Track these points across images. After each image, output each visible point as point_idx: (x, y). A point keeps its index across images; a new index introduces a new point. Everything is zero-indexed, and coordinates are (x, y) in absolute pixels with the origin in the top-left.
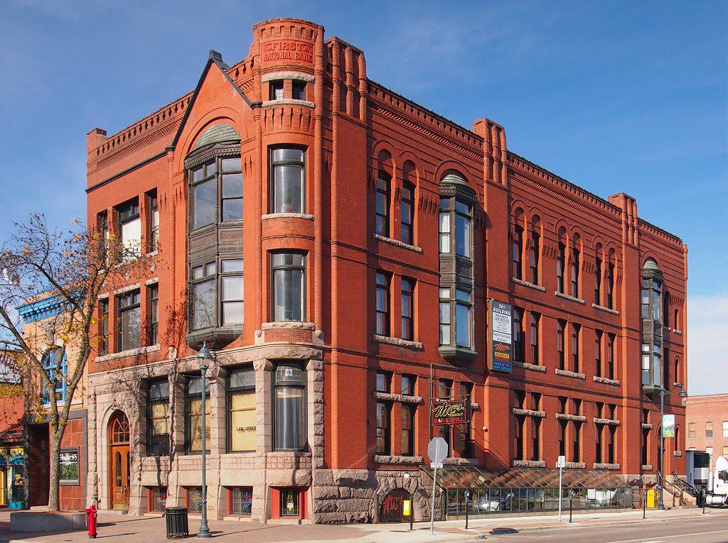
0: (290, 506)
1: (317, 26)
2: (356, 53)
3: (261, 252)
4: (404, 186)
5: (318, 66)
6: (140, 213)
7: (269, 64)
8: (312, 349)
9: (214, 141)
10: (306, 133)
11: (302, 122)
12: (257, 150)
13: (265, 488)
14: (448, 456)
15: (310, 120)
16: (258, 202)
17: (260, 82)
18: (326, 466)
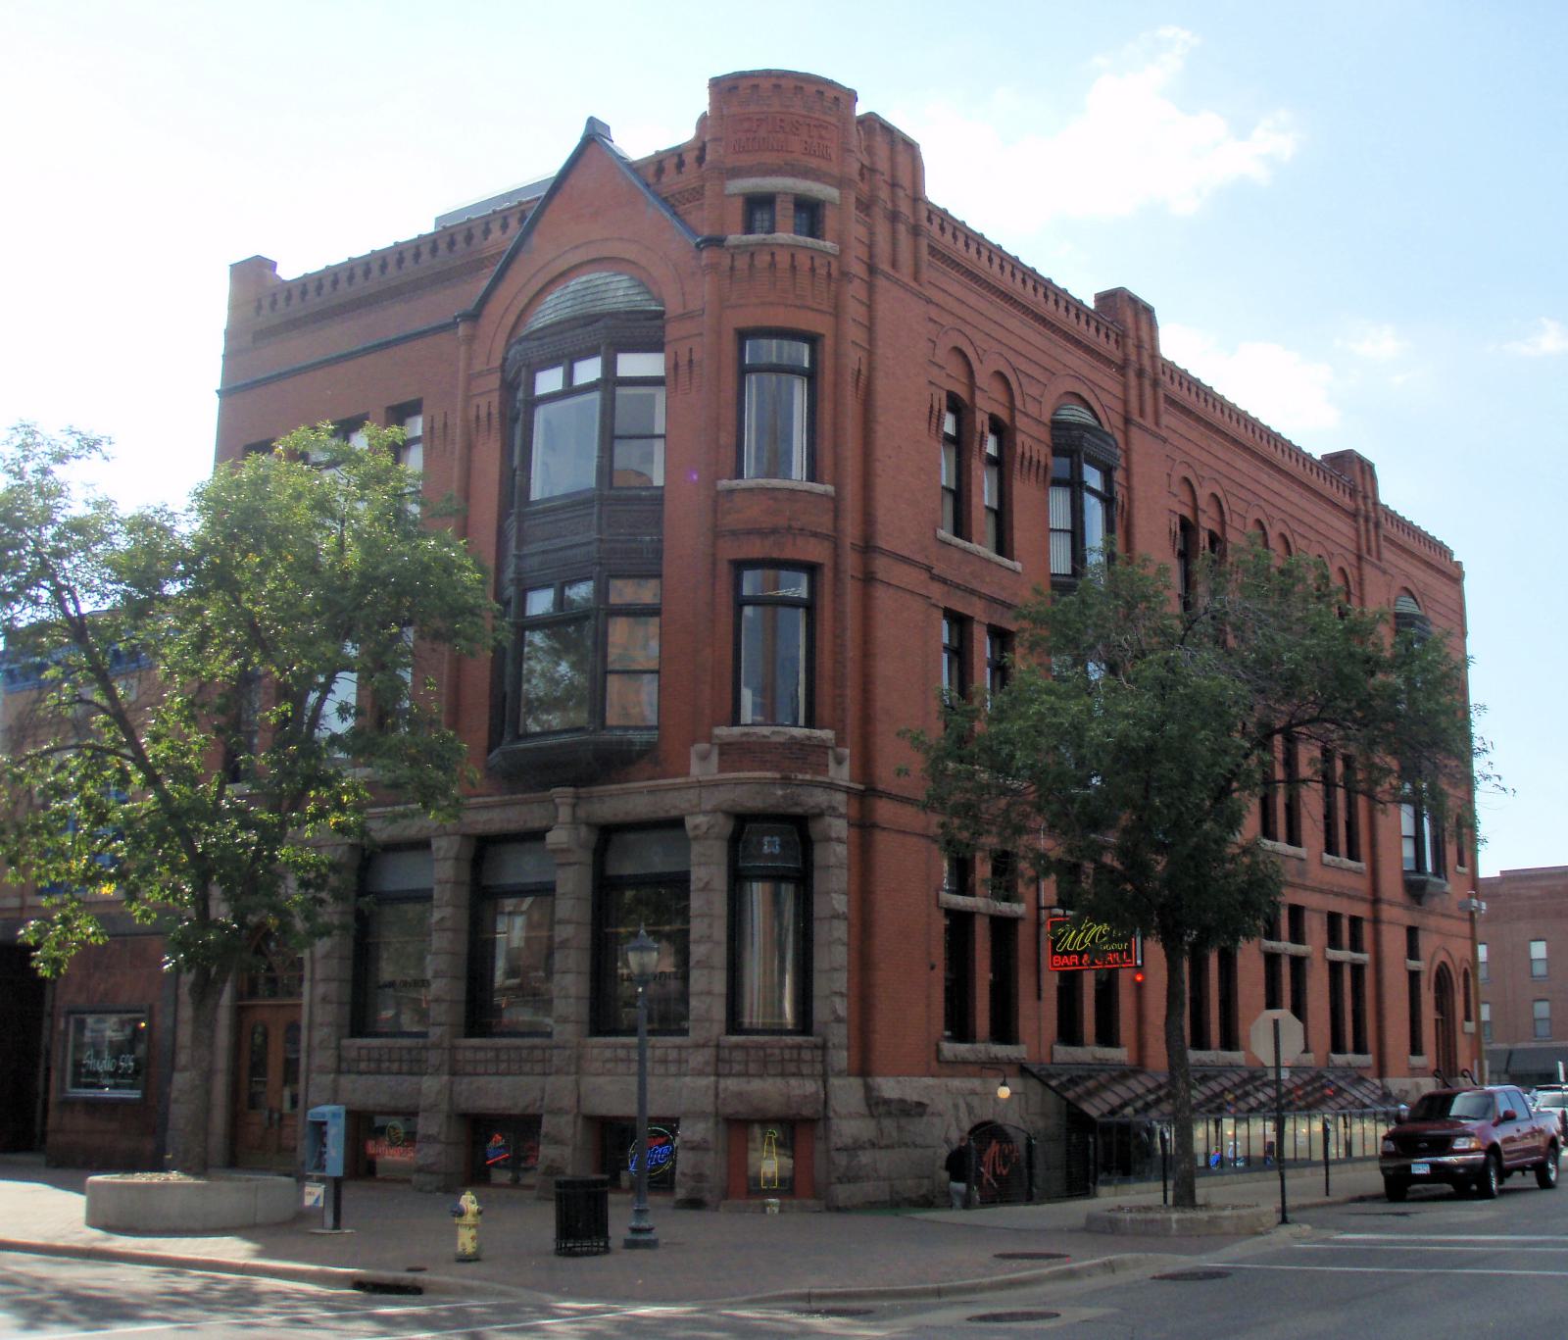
7: (746, 160)
14: (1306, 1050)
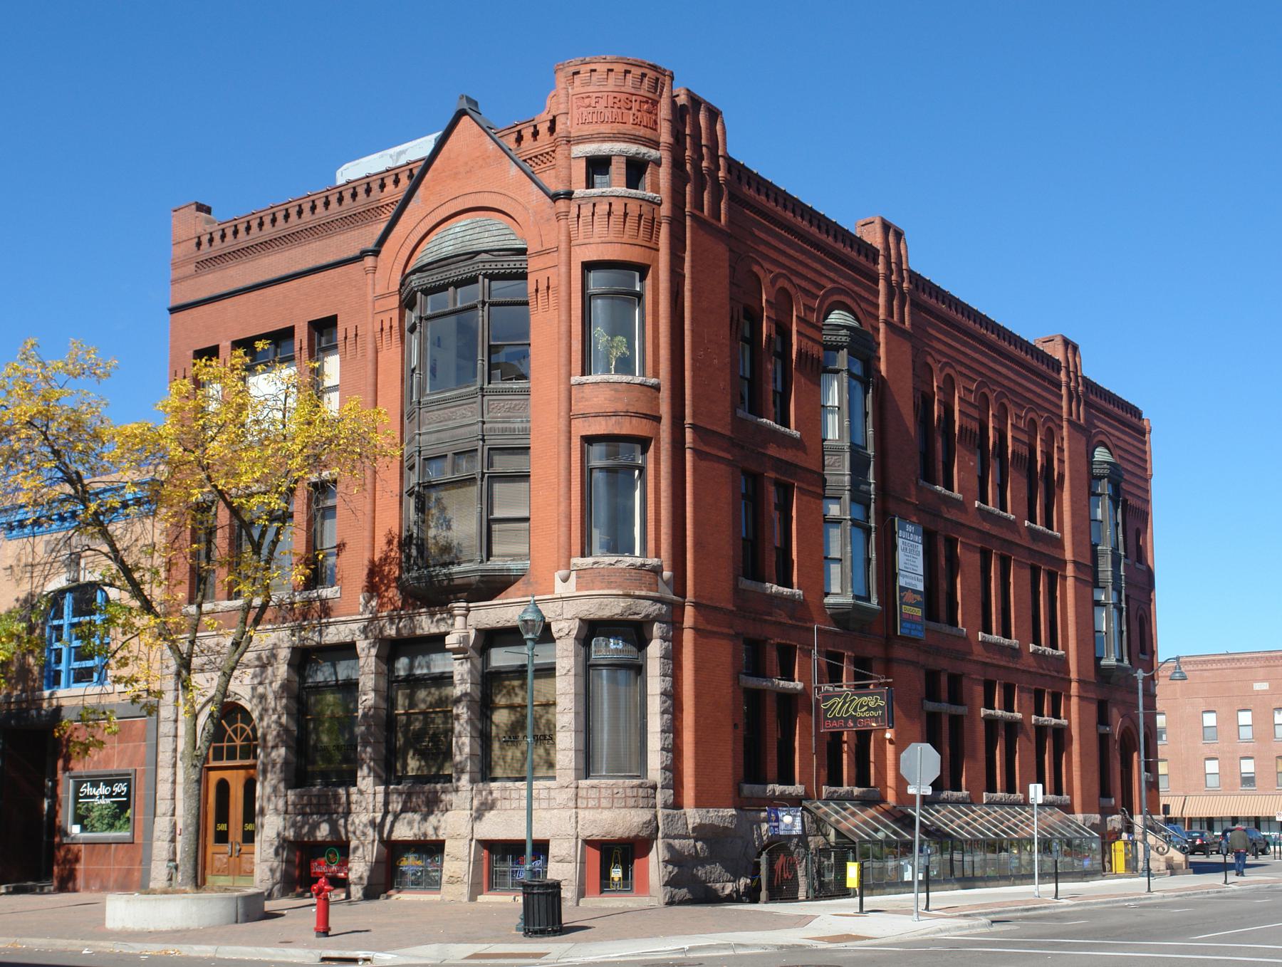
0: (616, 873)
1: (663, 72)
2: (714, 114)
3: (570, 439)
4: (777, 333)
5: (665, 136)
6: (297, 355)
7: (587, 130)
8: (659, 605)
9: (476, 248)
10: (648, 244)
11: (641, 229)
12: (563, 269)
13: (577, 842)
15: (653, 225)
16: (563, 353)
17: (569, 158)
18: (677, 804)
